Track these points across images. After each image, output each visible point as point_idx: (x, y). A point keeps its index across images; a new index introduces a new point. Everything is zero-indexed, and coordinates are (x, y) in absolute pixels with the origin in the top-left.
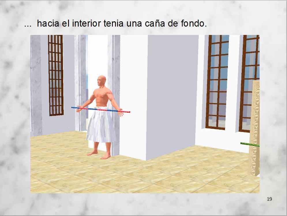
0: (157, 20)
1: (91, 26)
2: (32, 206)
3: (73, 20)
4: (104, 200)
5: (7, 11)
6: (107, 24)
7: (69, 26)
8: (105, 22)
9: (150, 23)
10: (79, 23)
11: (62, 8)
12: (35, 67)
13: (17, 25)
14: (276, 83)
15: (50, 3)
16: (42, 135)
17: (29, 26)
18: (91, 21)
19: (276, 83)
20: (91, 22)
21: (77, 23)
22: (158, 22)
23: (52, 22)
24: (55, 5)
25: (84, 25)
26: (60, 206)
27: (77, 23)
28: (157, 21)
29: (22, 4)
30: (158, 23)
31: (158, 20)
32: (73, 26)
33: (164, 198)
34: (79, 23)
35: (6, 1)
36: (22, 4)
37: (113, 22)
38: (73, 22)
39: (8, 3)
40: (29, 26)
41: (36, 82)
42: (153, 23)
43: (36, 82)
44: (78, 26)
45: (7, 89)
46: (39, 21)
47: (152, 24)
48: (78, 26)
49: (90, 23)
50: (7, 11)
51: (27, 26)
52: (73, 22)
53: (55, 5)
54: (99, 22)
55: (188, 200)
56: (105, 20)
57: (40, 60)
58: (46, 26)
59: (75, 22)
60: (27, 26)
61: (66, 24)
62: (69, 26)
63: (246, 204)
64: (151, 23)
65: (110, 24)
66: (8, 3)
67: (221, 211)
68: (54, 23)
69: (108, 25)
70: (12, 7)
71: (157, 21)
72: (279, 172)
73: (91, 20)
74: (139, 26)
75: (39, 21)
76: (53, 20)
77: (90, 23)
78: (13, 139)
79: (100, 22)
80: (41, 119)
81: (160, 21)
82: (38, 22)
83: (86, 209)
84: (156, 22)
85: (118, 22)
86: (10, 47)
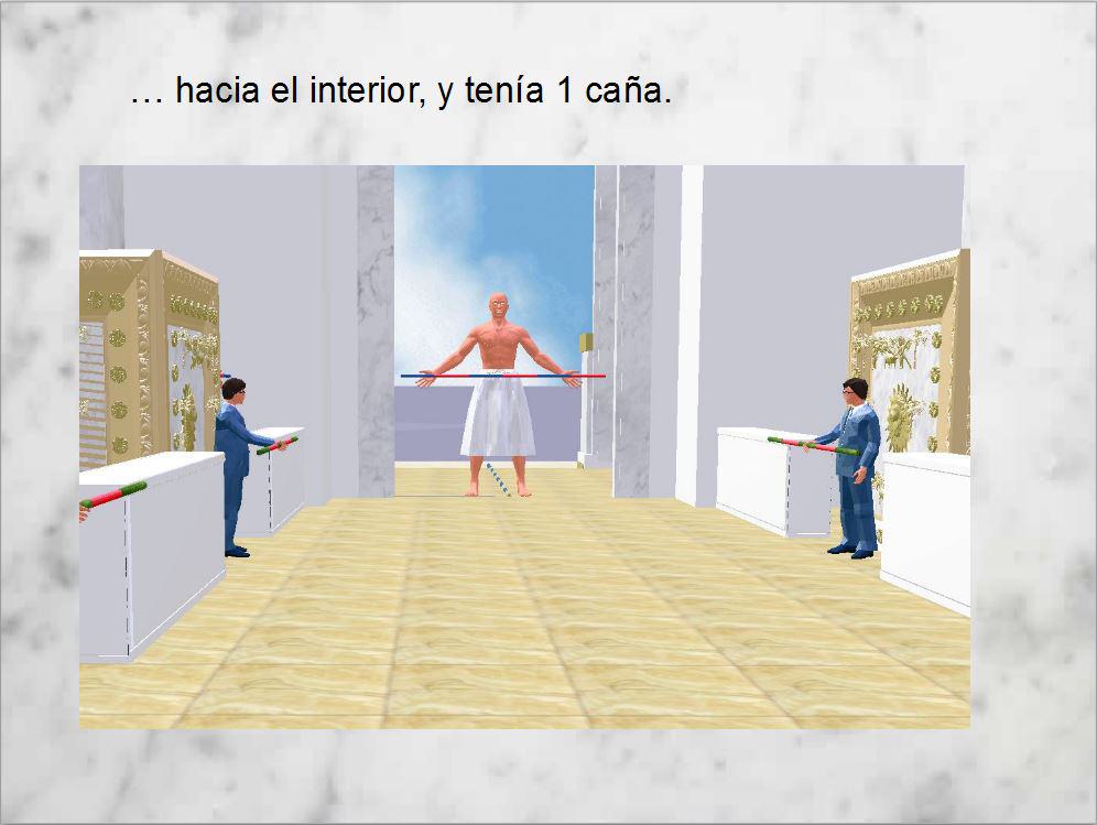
0: (631, 78)
1: (383, 101)
2: (125, 787)
3: (313, 78)
4: (400, 764)
5: (29, 43)
6: (350, 92)
7: (295, 101)
8: (469, 84)
9: (603, 92)
10: (337, 89)
11: (238, 30)
12: (632, 244)
13: (68, 98)
14: (1055, 318)
15: (192, 13)
16: (647, 496)
17: (141, 101)
18: (383, 81)
19: (1055, 318)
20: (383, 84)
21: (327, 90)
22: (633, 84)
23: (234, 87)
24: (215, 18)
25: (355, 96)
26: (231, 788)
27: (327, 90)
28: (632, 81)
29: (86, 16)
30: (633, 90)
31: (637, 79)
32: (313, 101)
33: (628, 755)
34: (337, 89)
35: (27, 5)
36: (86, 16)
37: (499, 86)
38: (313, 84)
39: (35, 13)
40: (141, 101)
41: (636, 297)
42: (617, 91)
43: (636, 297)
44: (333, 101)
45: (33, 338)
46: (182, 83)
47: (613, 94)
48: (333, 101)
49: (377, 90)
50: (29, 43)
51: (153, 101)
52: (313, 84)
53: (215, 18)
54: (412, 86)
55: (720, 765)
56: (469, 79)
57: (652, 217)
58: (209, 99)
59: (322, 86)
60: (153, 101)
61: (286, 92)
62: (295, 101)
63: (943, 780)
64: (607, 90)
65: (362, 91)
66: (35, 13)
67: (845, 805)
68: (242, 91)
69: (354, 96)
70: (49, 27)
71: (632, 81)
72: (1068, 659)
73: (383, 78)
74: (203, 101)
75: (182, 83)
76: (237, 78)
77: (377, 90)
78: (51, 531)
79: (418, 84)
80: (647, 438)
81: (642, 83)
82: (180, 87)
83: (331, 797)
84: (628, 86)
85: (241, 86)
86: (42, 179)
